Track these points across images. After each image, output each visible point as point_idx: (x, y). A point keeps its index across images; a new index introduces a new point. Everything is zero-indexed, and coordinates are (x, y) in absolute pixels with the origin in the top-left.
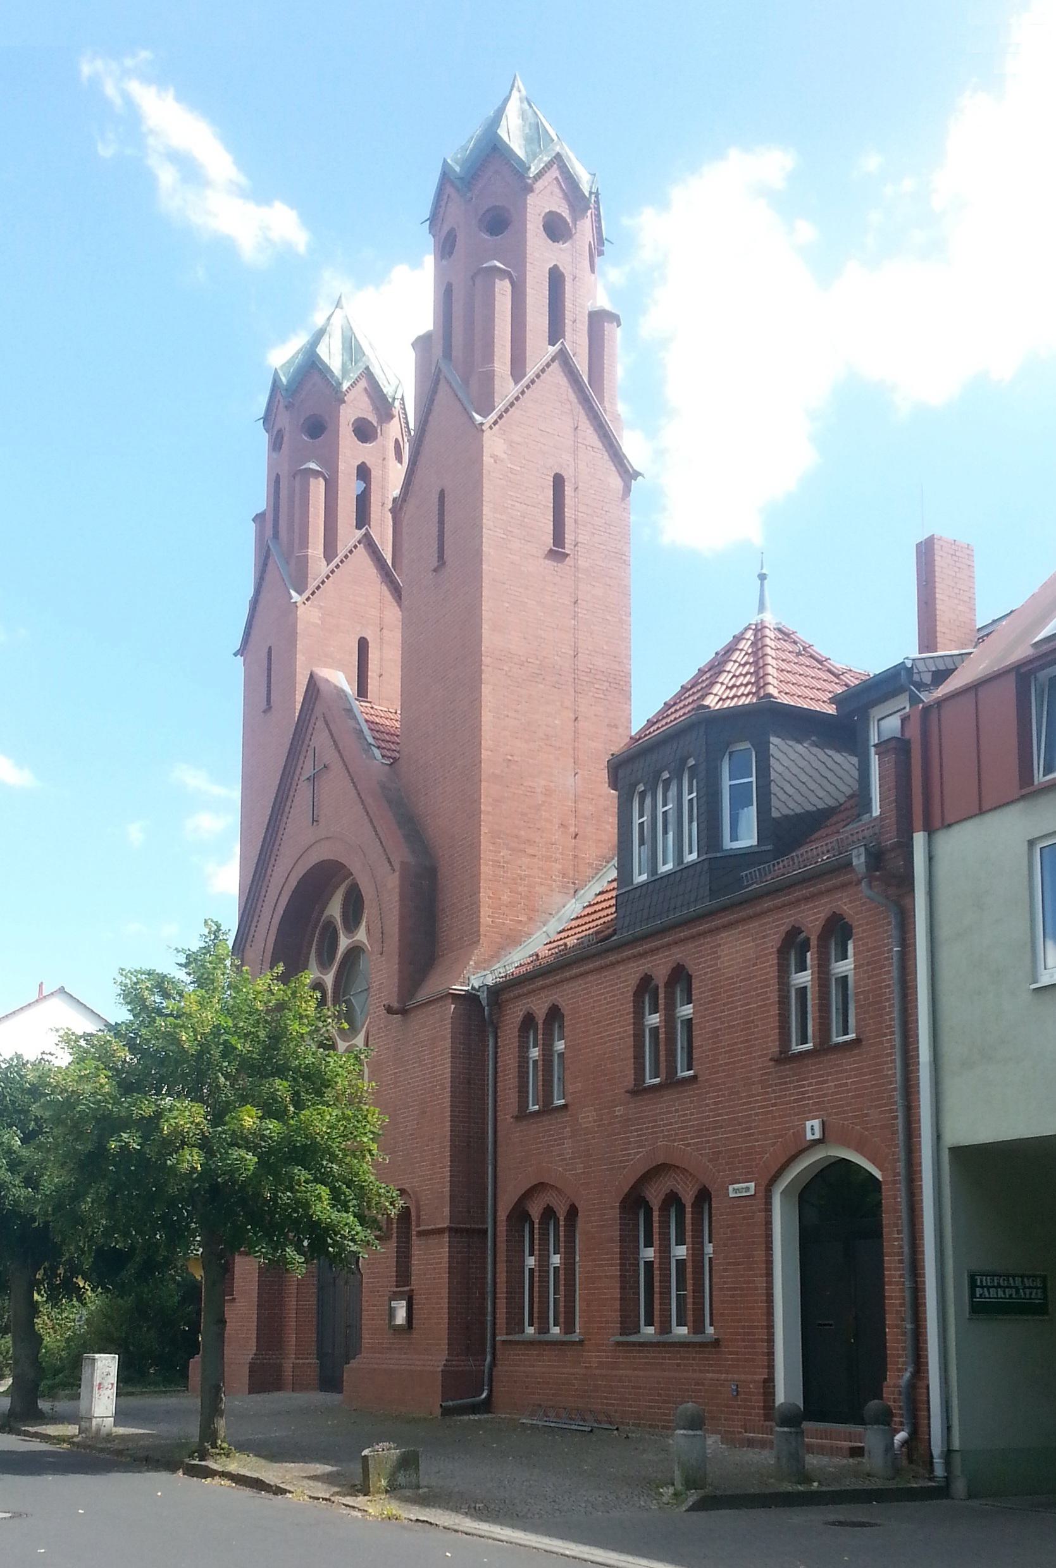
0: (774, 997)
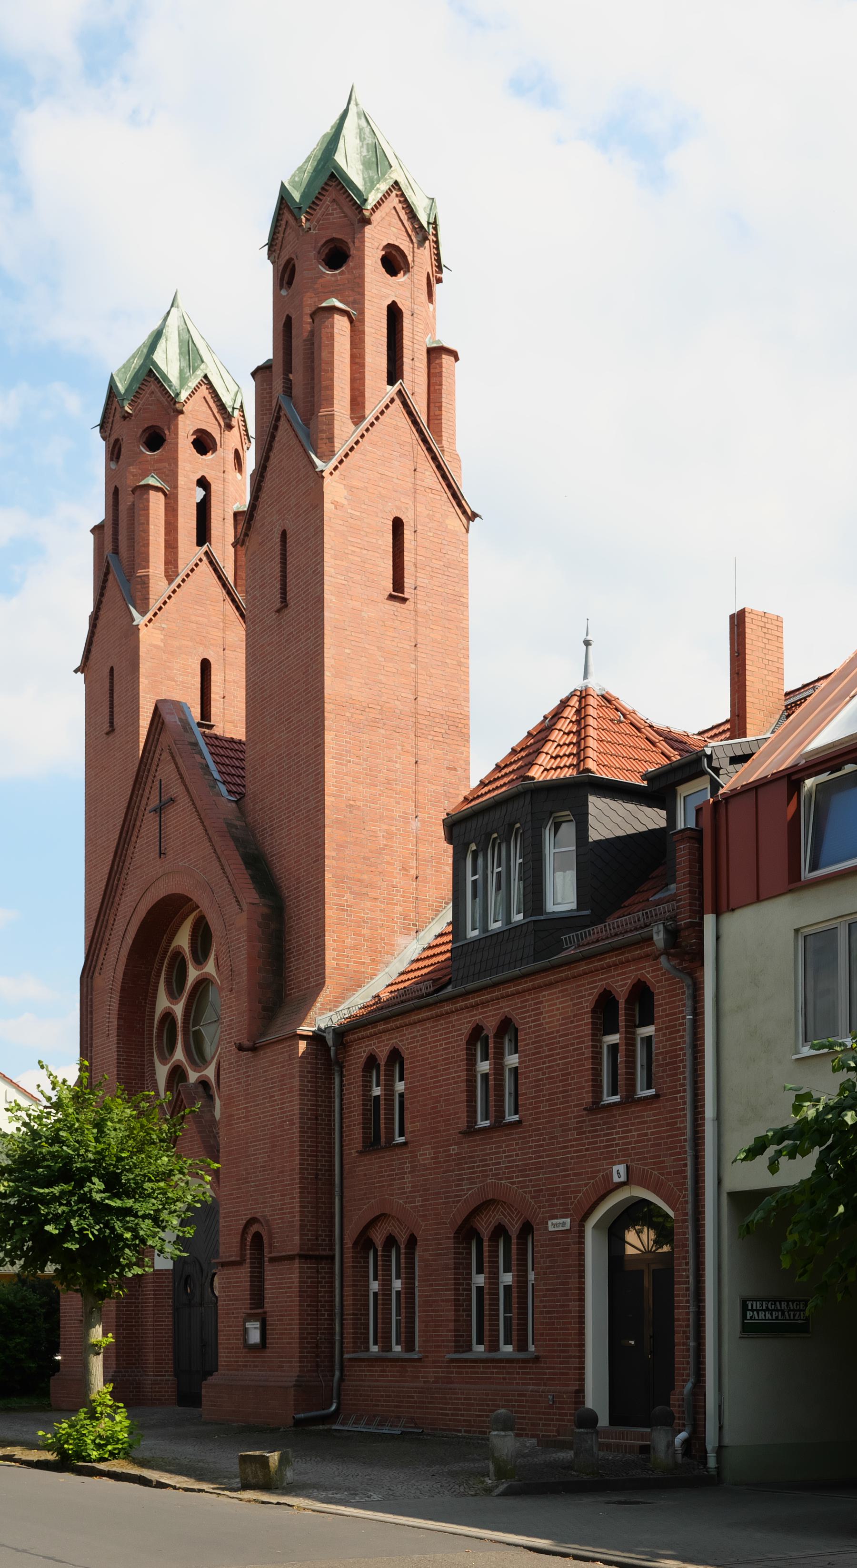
0: (588, 1053)
